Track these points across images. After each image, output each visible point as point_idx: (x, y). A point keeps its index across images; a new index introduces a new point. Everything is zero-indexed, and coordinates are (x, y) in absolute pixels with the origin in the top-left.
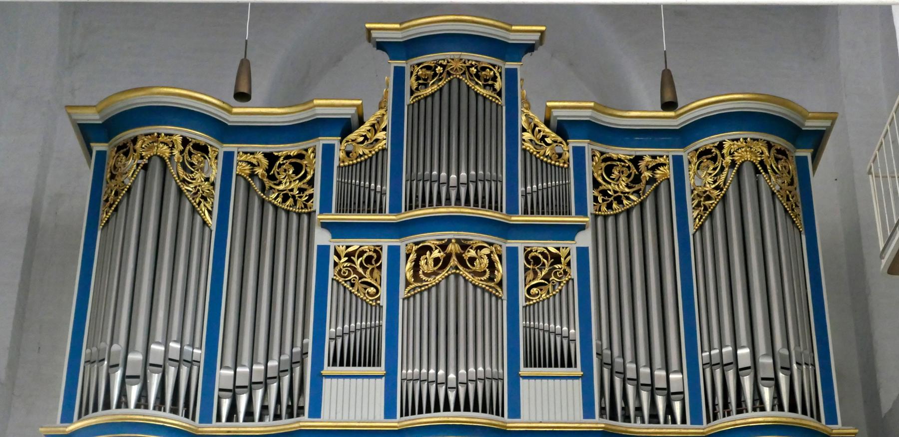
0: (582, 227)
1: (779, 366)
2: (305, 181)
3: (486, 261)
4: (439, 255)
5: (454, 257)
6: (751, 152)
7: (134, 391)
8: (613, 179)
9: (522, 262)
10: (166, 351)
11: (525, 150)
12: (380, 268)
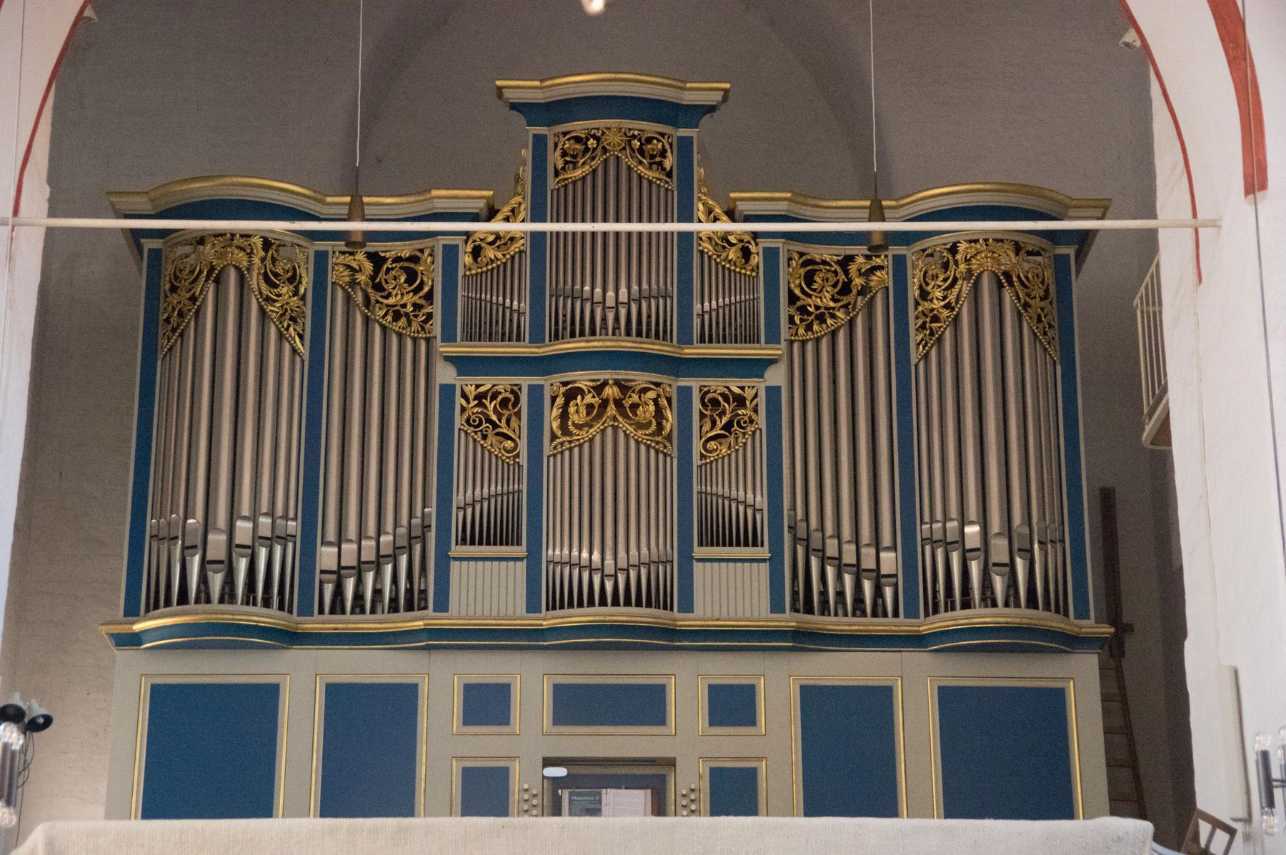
0: (772, 362)
1: (1016, 548)
2: (422, 294)
3: (652, 408)
4: (593, 401)
5: (612, 405)
6: (993, 258)
7: (217, 581)
8: (814, 290)
9: (697, 405)
10: (255, 528)
11: (702, 252)
12: (518, 414)
